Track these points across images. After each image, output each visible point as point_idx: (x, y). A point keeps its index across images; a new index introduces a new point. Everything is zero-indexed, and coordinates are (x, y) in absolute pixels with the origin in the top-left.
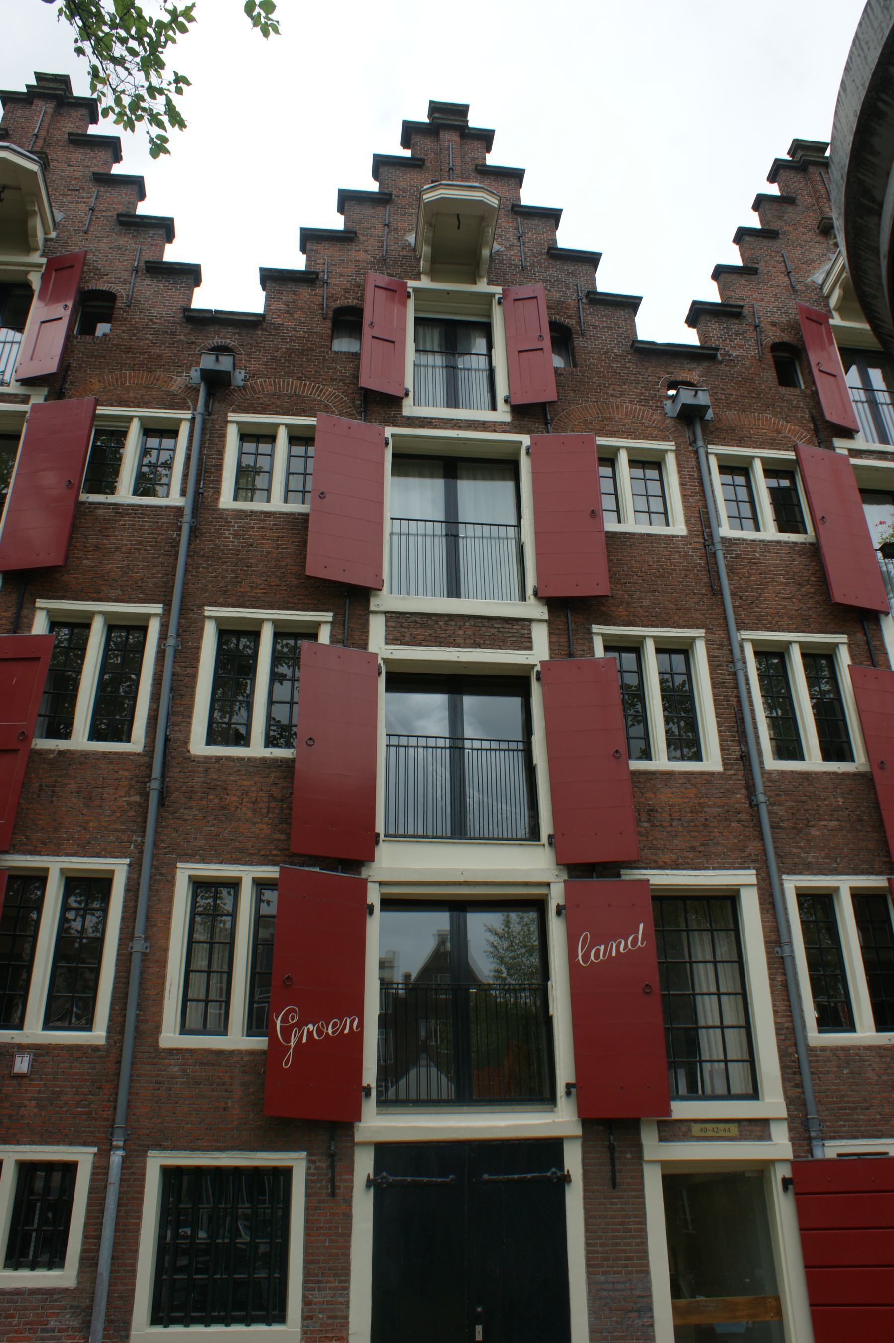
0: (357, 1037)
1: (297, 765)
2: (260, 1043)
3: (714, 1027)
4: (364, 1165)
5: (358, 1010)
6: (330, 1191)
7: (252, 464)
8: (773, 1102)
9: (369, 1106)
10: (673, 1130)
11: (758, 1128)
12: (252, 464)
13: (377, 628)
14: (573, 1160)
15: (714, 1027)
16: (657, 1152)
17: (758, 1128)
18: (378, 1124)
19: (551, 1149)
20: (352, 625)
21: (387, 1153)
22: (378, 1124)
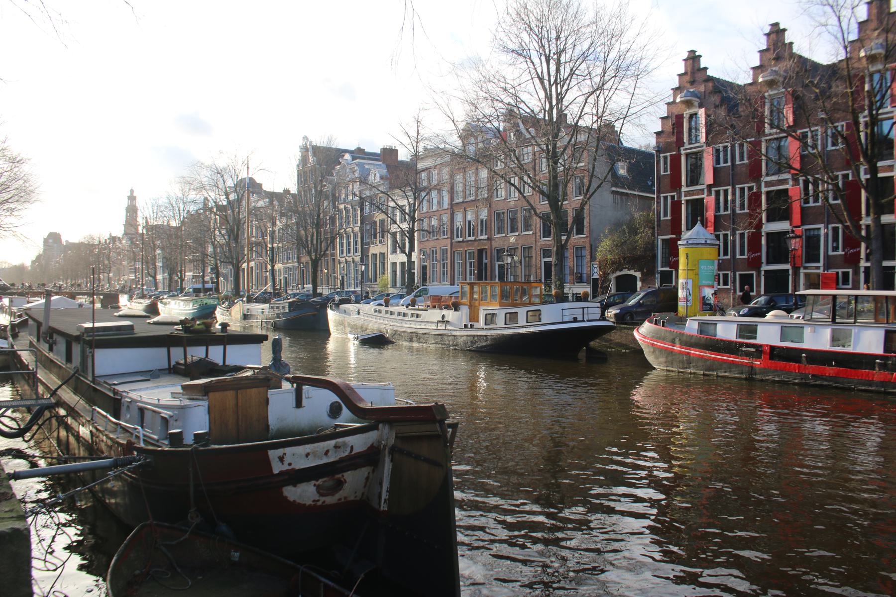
0: (760, 257)
1: (786, 33)
2: (836, 124)
3: (60, 387)
4: (763, 273)
5: (760, 251)
6: (759, 276)
7: (183, 362)
8: (821, 264)
9: (764, 265)
10: (806, 268)
11: (818, 268)
12: (183, 362)
13: (763, 184)
14: (790, 272)
15: (60, 387)
16: (802, 271)
17: (818, 268)
18: (765, 267)
19: (787, 270)
20: (813, 129)
21: (766, 271)
22: (765, 267)
